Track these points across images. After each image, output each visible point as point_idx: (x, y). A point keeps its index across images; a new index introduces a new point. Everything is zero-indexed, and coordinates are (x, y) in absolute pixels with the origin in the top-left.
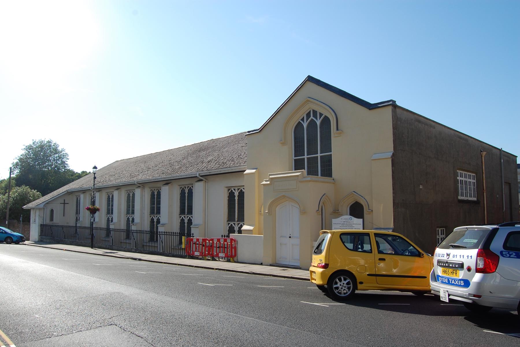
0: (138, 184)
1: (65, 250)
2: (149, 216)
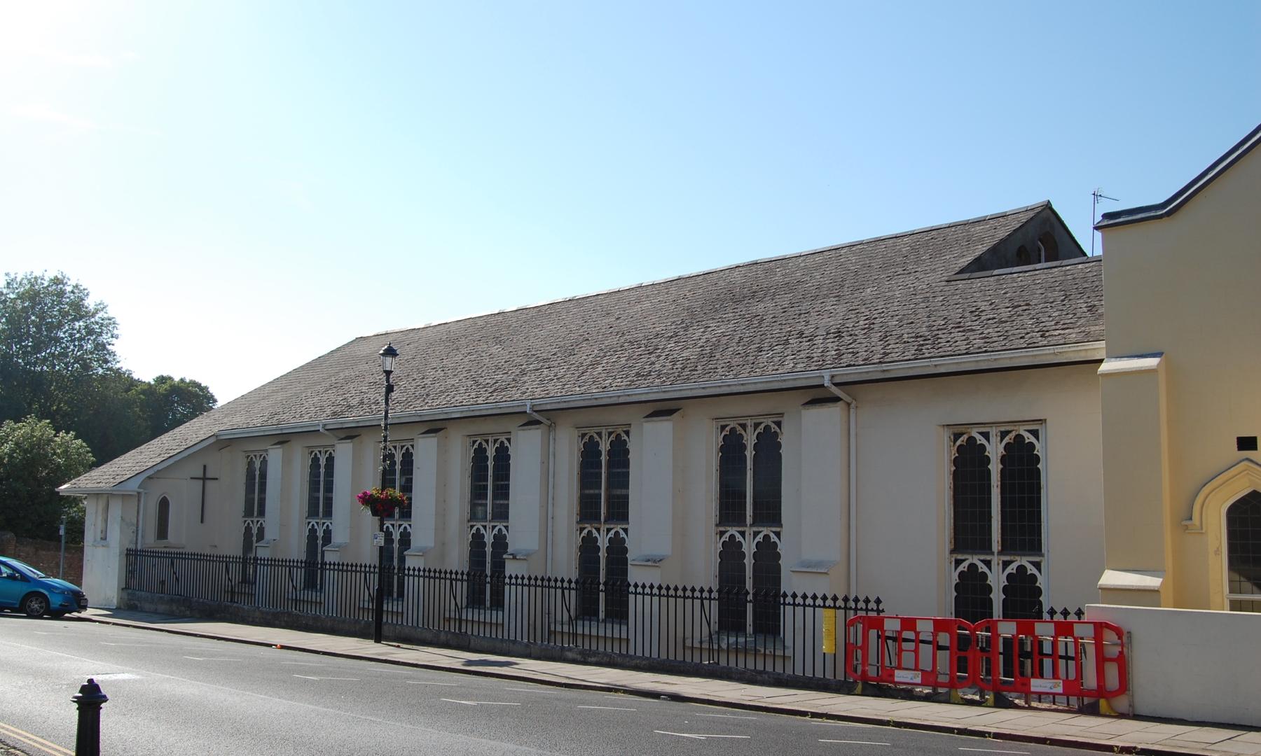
0: (536, 411)
1: (283, 647)
2: (575, 526)
